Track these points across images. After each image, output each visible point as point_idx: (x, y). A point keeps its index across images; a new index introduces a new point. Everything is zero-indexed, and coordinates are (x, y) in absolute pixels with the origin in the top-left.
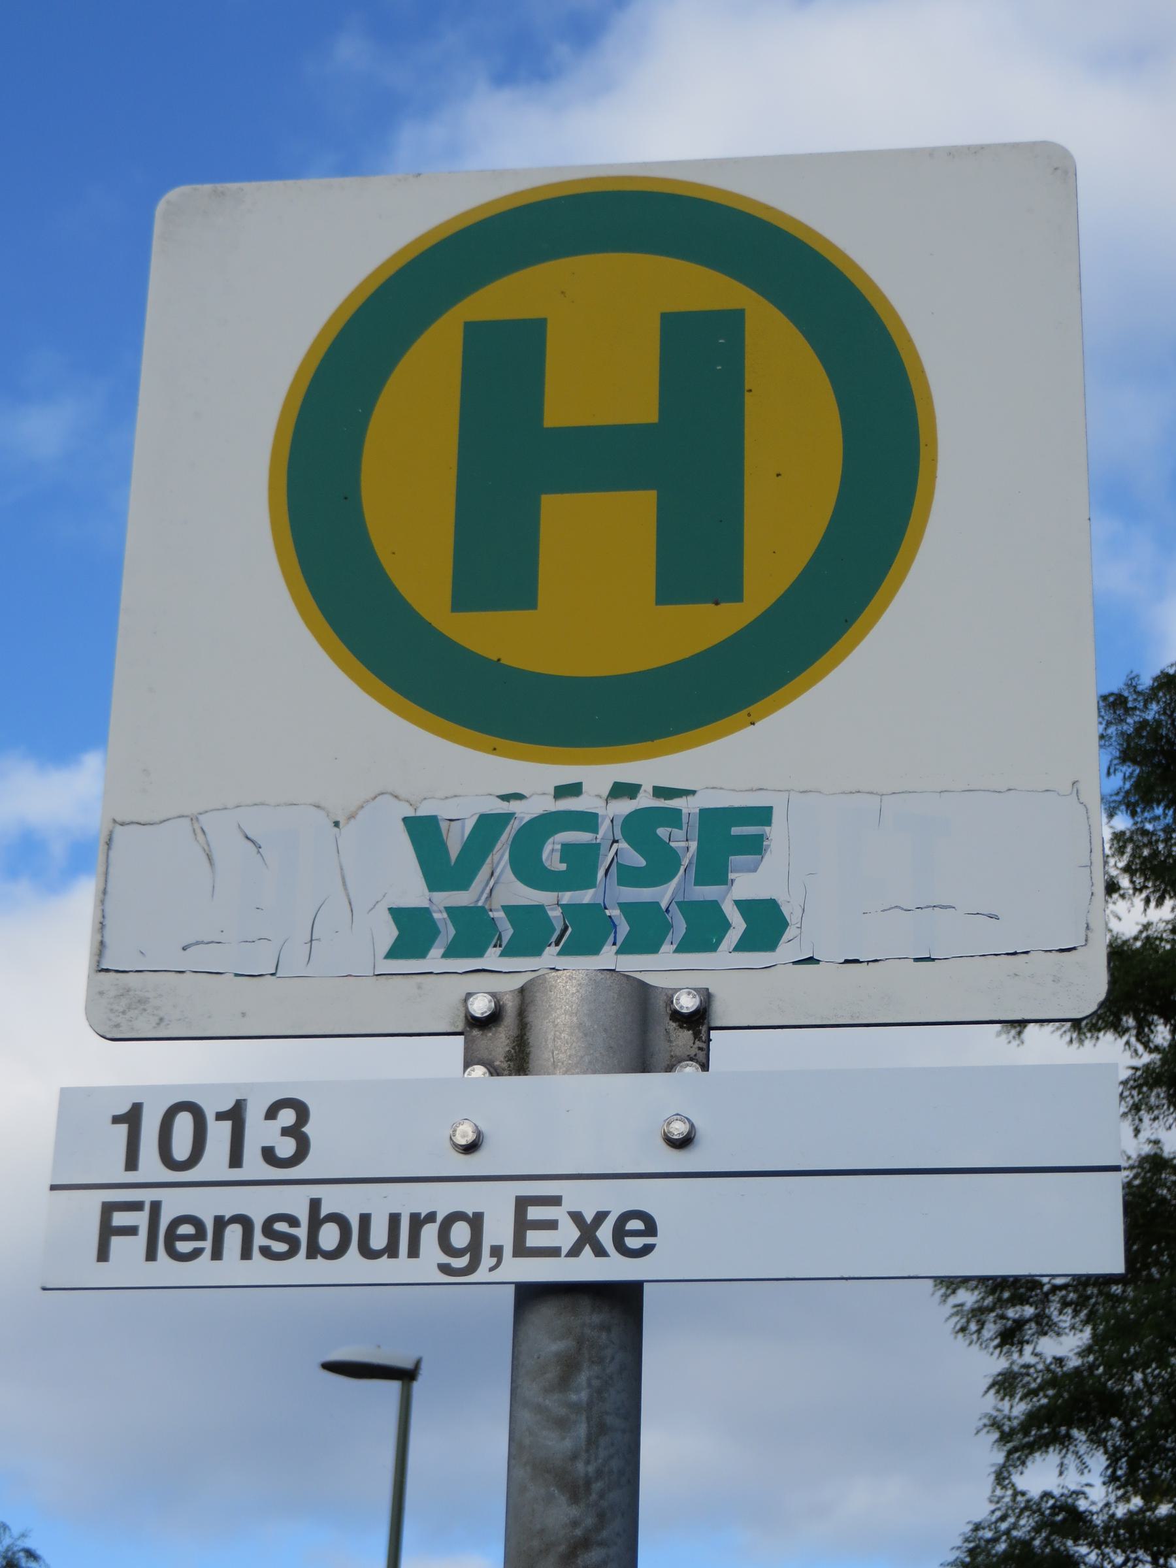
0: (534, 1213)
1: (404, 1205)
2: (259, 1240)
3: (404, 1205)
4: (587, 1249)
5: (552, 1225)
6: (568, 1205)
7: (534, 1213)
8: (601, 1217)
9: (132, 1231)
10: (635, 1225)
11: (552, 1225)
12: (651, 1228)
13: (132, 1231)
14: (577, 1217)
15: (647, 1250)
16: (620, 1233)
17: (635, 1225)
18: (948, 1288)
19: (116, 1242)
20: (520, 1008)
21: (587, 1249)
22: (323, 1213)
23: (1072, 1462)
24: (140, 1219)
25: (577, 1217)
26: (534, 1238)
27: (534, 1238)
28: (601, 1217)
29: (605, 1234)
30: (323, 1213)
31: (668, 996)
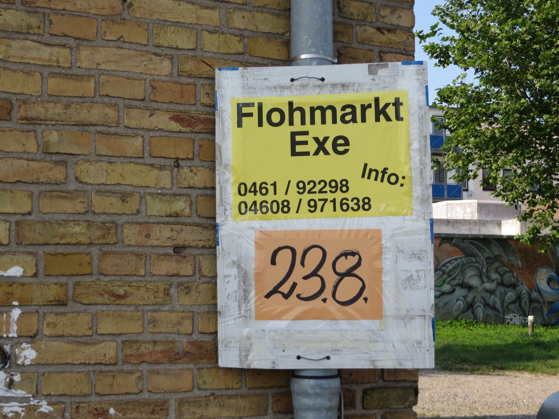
0: (298, 138)
1: (110, 204)
2: (339, 113)
3: (110, 204)
4: (321, 152)
5: (305, 143)
6: (312, 134)
7: (298, 138)
8: (326, 139)
9: (250, 115)
10: (341, 141)
11: (305, 143)
12: (347, 143)
13: (250, 115)
14: (316, 139)
15: (346, 151)
16: (335, 145)
17: (341, 141)
18: (352, 26)
19: (244, 119)
20: (290, 21)
21: (321, 152)
22: (294, 107)
23: (517, 261)
24: (254, 110)
25: (316, 139)
26: (299, 149)
27: (299, 149)
28: (326, 139)
29: (328, 146)
30: (294, 107)
31: (441, 244)
